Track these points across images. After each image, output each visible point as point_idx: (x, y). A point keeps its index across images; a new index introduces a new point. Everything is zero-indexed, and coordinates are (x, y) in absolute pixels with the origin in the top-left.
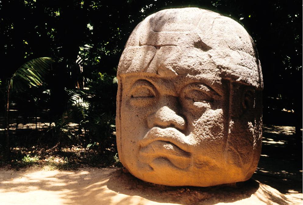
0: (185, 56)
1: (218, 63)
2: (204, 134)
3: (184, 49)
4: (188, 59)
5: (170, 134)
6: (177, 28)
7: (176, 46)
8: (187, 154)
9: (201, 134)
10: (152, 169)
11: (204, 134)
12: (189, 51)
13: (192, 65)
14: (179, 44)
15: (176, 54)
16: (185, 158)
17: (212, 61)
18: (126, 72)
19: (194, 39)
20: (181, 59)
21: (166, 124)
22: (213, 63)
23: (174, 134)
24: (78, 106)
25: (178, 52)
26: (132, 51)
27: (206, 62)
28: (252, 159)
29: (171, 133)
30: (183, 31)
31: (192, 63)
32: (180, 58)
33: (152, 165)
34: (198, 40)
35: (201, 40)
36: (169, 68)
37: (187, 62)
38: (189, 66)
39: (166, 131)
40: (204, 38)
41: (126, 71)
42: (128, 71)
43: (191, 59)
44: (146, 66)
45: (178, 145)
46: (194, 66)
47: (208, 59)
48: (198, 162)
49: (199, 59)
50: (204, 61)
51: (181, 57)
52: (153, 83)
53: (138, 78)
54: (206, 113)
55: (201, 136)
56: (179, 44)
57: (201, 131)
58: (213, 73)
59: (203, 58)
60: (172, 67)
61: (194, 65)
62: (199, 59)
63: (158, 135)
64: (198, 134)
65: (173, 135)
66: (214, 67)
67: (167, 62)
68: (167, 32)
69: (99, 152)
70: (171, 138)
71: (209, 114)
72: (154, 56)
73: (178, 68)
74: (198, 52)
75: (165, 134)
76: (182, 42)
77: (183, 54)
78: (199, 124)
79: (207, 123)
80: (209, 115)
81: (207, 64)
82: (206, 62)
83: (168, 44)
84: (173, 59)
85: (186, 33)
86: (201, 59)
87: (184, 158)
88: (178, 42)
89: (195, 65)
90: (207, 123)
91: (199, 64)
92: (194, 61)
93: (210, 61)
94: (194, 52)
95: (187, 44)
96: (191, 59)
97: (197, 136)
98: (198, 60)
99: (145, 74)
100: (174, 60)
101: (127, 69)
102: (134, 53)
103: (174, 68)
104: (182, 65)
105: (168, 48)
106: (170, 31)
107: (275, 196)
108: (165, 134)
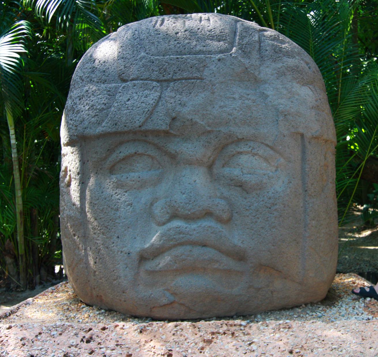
6: (198, 48)
30: (210, 52)
68: (179, 57)
79: (270, 208)
85: (217, 58)
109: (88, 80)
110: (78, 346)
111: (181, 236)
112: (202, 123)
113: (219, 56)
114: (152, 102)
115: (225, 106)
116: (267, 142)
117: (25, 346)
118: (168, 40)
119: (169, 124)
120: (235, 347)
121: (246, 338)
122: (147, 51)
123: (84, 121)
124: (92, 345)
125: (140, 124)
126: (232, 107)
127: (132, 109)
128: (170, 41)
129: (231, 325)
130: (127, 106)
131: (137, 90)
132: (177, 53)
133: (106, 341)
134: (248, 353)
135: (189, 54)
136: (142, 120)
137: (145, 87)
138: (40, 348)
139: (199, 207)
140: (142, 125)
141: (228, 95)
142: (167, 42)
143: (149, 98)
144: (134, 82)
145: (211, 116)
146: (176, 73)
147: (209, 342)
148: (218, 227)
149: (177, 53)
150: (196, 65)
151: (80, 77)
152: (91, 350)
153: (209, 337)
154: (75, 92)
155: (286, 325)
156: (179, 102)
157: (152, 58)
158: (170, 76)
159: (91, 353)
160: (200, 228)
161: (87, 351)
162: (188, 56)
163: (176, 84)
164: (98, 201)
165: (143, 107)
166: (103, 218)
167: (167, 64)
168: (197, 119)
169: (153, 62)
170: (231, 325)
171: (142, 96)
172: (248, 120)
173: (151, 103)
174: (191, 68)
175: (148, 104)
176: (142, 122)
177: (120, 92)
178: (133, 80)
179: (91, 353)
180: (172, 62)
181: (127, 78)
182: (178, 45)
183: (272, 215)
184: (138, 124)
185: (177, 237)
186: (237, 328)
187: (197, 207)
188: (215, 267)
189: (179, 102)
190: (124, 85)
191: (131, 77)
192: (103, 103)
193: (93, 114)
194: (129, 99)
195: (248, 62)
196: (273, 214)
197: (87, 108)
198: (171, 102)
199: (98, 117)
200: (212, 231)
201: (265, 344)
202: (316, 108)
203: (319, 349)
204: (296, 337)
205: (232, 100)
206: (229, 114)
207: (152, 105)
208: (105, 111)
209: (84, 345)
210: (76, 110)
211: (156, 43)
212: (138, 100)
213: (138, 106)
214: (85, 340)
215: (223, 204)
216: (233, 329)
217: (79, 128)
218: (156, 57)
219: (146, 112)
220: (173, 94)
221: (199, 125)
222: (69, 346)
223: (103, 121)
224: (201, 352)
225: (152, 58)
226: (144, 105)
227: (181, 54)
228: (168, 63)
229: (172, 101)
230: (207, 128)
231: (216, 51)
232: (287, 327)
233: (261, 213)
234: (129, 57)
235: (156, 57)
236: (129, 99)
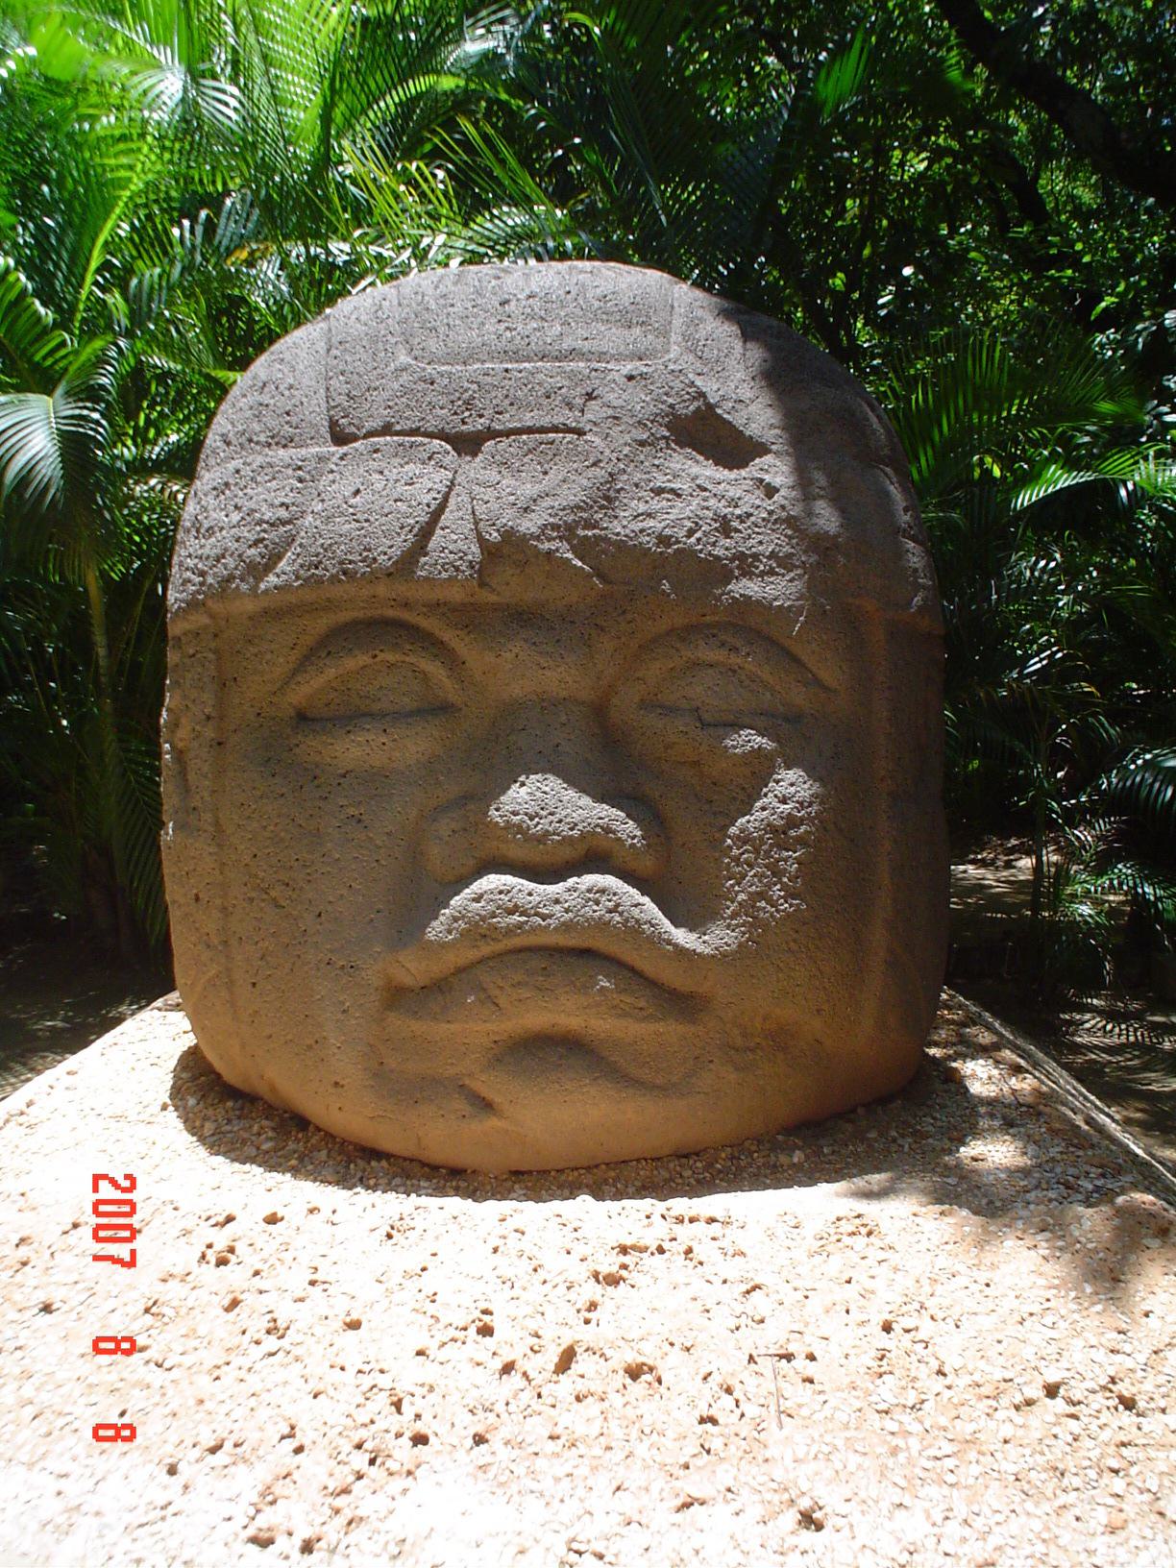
0: (637, 485)
3: (626, 450)
4: (656, 504)
5: (595, 908)
6: (567, 344)
7: (580, 433)
8: (681, 1003)
9: (761, 895)
10: (486, 1106)
12: (656, 462)
14: (595, 424)
15: (590, 474)
16: (681, 1029)
18: (262, 586)
19: (671, 401)
21: (568, 853)
23: (618, 905)
24: (1144, 793)
25: (594, 464)
26: (290, 472)
27: (752, 519)
29: (597, 903)
30: (602, 356)
31: (677, 523)
32: (612, 494)
33: (488, 1085)
34: (696, 404)
35: (711, 407)
38: (664, 540)
39: (566, 896)
40: (723, 398)
41: (259, 579)
42: (272, 579)
43: (669, 500)
44: (408, 544)
45: (647, 967)
46: (693, 540)
47: (758, 502)
48: (739, 1041)
49: (712, 502)
50: (738, 512)
51: (618, 491)
52: (447, 635)
53: (323, 623)
54: (777, 782)
56: (595, 424)
57: (760, 876)
58: (792, 574)
59: (731, 494)
61: (691, 533)
62: (712, 502)
64: (742, 897)
65: (610, 911)
67: (540, 522)
68: (510, 366)
70: (602, 925)
71: (792, 785)
72: (450, 488)
73: (603, 552)
74: (694, 469)
75: (567, 911)
76: (610, 412)
77: (625, 477)
78: (745, 843)
80: (792, 789)
82: (749, 515)
83: (529, 424)
84: (573, 500)
85: (625, 371)
87: (671, 1030)
88: (589, 416)
89: (698, 535)
90: (784, 833)
91: (716, 529)
92: (687, 513)
93: (771, 513)
94: (679, 466)
95: (639, 422)
96: (669, 500)
97: (740, 904)
98: (707, 508)
99: (402, 589)
101: (268, 568)
102: (301, 481)
103: (582, 548)
104: (628, 531)
105: (531, 445)
106: (529, 360)
108: (567, 911)
109: (243, 440)
110: (189, 1278)
111: (516, 918)
113: (629, 367)
114: (427, 498)
117: (27, 1269)
118: (479, 320)
120: (698, 1306)
121: (733, 1269)
122: (415, 352)
123: (224, 557)
124: (234, 1277)
127: (367, 521)
128: (483, 324)
129: (680, 1220)
130: (351, 510)
131: (384, 465)
132: (506, 355)
133: (278, 1263)
134: (743, 1328)
135: (542, 359)
137: (405, 453)
138: (75, 1277)
139: (572, 829)
141: (660, 481)
142: (474, 326)
143: (417, 486)
144: (376, 439)
146: (500, 413)
147: (613, 1280)
149: (506, 355)
150: (564, 390)
151: (223, 435)
152: (230, 1297)
153: (609, 1264)
154: (207, 476)
155: (857, 1221)
157: (429, 369)
158: (482, 420)
159: (228, 1309)
160: (576, 894)
161: (215, 1299)
162: (540, 364)
163: (500, 447)
167: (475, 387)
169: (432, 383)
170: (680, 1220)
171: (397, 481)
174: (548, 397)
177: (332, 471)
178: (371, 434)
179: (228, 1309)
180: (488, 379)
181: (353, 429)
182: (508, 334)
186: (700, 1227)
190: (344, 449)
191: (369, 425)
193: (252, 537)
194: (358, 492)
195: (715, 388)
197: (235, 517)
198: (486, 498)
201: (799, 1295)
203: (979, 1319)
204: (896, 1270)
205: (670, 497)
207: (428, 506)
209: (209, 1271)
210: (206, 526)
211: (442, 330)
212: (384, 493)
213: (386, 511)
214: (211, 1256)
216: (685, 1232)
217: (210, 580)
218: (443, 368)
220: (492, 475)
222: (161, 1276)
223: (280, 557)
224: (587, 1322)
225: (429, 369)
227: (516, 356)
228: (478, 383)
229: (490, 494)
231: (620, 354)
232: (864, 1231)
234: (361, 370)
235: (443, 368)
236: (358, 492)
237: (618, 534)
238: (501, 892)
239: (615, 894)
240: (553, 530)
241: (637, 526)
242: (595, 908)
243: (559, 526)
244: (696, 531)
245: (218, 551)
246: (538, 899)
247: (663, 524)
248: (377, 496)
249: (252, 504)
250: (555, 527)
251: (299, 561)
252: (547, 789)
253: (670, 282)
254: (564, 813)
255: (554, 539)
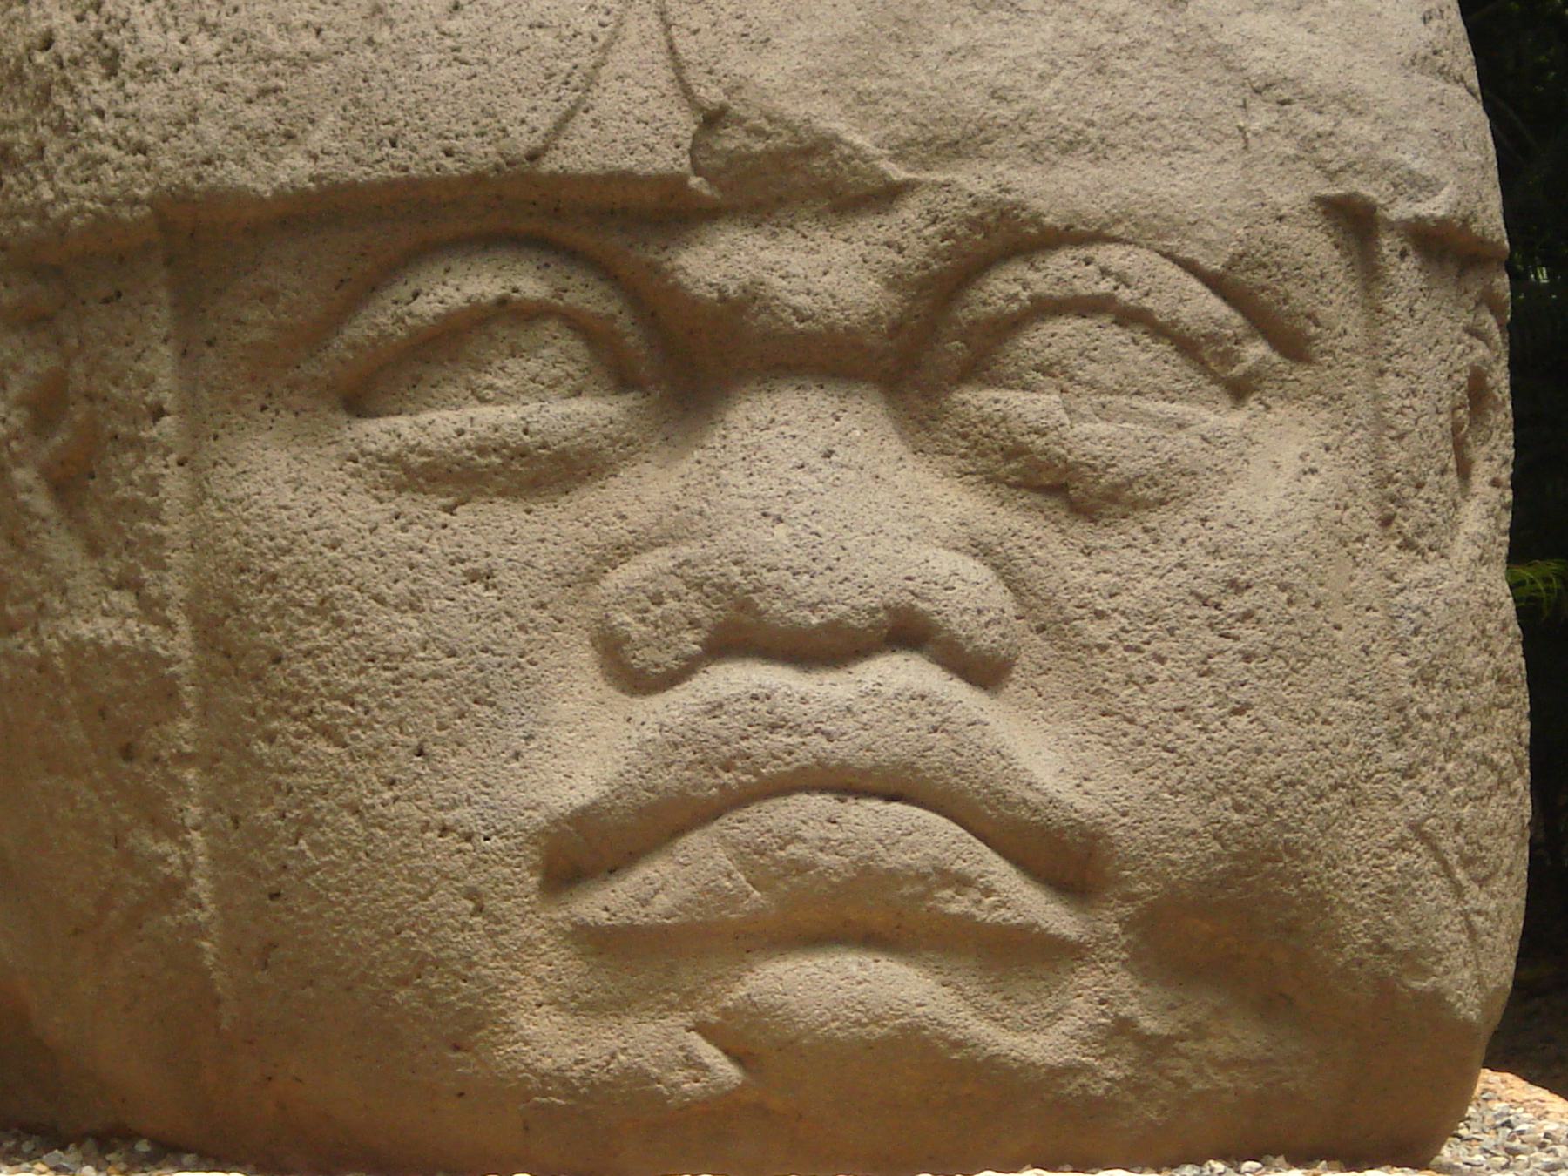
1: (1260, 62)
2: (1205, 706)
5: (911, 724)
11: (1205, 706)
13: (1026, 83)
17: (1204, 43)
20: (915, 30)
22: (1210, 52)
28: (162, 364)
36: (820, 115)
37: (974, 51)
46: (1047, 93)
50: (1123, 40)
55: (1184, 727)
60: (838, 109)
62: (1079, 26)
63: (796, 739)
66: (1223, 90)
69: (52, 203)
79: (1217, 606)
80: (1229, 534)
81: (1157, 71)
86: (1097, 23)
89: (1056, 84)
100: (857, 39)
107: (783, 666)
112: (859, 140)
115: (974, 51)
116: (1192, 251)
119: (687, 144)
125: (536, 141)
126: (1010, 54)
130: (449, 42)
136: (544, 122)
140: (546, 148)
145: (904, 106)
148: (959, 692)
156: (739, 26)
160: (878, 702)
164: (288, 559)
165: (540, 48)
166: (327, 650)
168: (832, 119)
172: (1091, 124)
173: (586, 29)
175: (568, 33)
176: (543, 129)
183: (1230, 642)
184: (523, 141)
185: (757, 745)
187: (854, 592)
188: (954, 908)
189: (739, 26)
192: (306, 25)
193: (252, 87)
196: (1236, 639)
199: (286, 103)
200: (934, 720)
202: (1426, 62)
206: (993, 95)
208: (324, 68)
213: (517, 44)
215: (974, 578)
219: (560, 78)
221: (847, 151)
226: (547, 39)
230: (885, 165)
233: (1171, 631)
237: (920, 86)
238: (755, 697)
239: (940, 703)
240: (812, 78)
241: (949, 72)
242: (911, 724)
243: (821, 73)
244: (1051, 77)
245: (179, 109)
246: (817, 707)
247: (995, 68)
248: (495, 17)
249: (240, 22)
250: (814, 75)
251: (358, 132)
252: (820, 529)
253: (1044, 899)
254: (851, 569)
255: (813, 96)
